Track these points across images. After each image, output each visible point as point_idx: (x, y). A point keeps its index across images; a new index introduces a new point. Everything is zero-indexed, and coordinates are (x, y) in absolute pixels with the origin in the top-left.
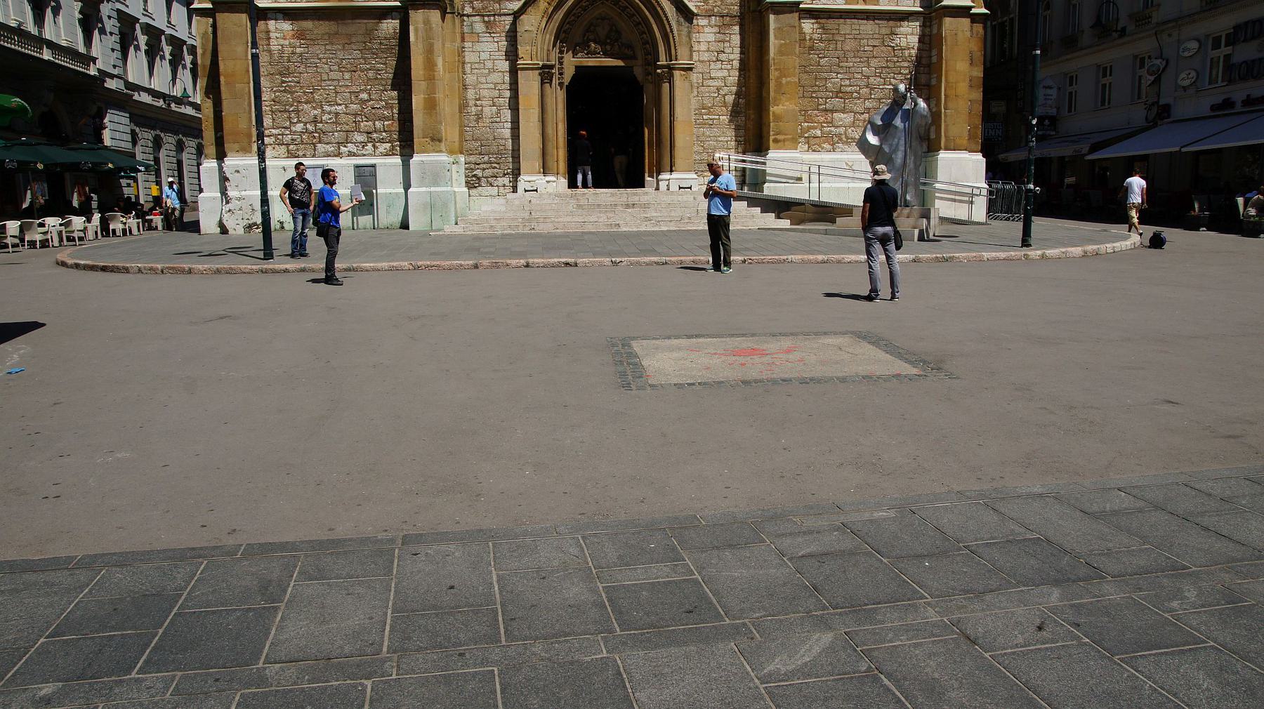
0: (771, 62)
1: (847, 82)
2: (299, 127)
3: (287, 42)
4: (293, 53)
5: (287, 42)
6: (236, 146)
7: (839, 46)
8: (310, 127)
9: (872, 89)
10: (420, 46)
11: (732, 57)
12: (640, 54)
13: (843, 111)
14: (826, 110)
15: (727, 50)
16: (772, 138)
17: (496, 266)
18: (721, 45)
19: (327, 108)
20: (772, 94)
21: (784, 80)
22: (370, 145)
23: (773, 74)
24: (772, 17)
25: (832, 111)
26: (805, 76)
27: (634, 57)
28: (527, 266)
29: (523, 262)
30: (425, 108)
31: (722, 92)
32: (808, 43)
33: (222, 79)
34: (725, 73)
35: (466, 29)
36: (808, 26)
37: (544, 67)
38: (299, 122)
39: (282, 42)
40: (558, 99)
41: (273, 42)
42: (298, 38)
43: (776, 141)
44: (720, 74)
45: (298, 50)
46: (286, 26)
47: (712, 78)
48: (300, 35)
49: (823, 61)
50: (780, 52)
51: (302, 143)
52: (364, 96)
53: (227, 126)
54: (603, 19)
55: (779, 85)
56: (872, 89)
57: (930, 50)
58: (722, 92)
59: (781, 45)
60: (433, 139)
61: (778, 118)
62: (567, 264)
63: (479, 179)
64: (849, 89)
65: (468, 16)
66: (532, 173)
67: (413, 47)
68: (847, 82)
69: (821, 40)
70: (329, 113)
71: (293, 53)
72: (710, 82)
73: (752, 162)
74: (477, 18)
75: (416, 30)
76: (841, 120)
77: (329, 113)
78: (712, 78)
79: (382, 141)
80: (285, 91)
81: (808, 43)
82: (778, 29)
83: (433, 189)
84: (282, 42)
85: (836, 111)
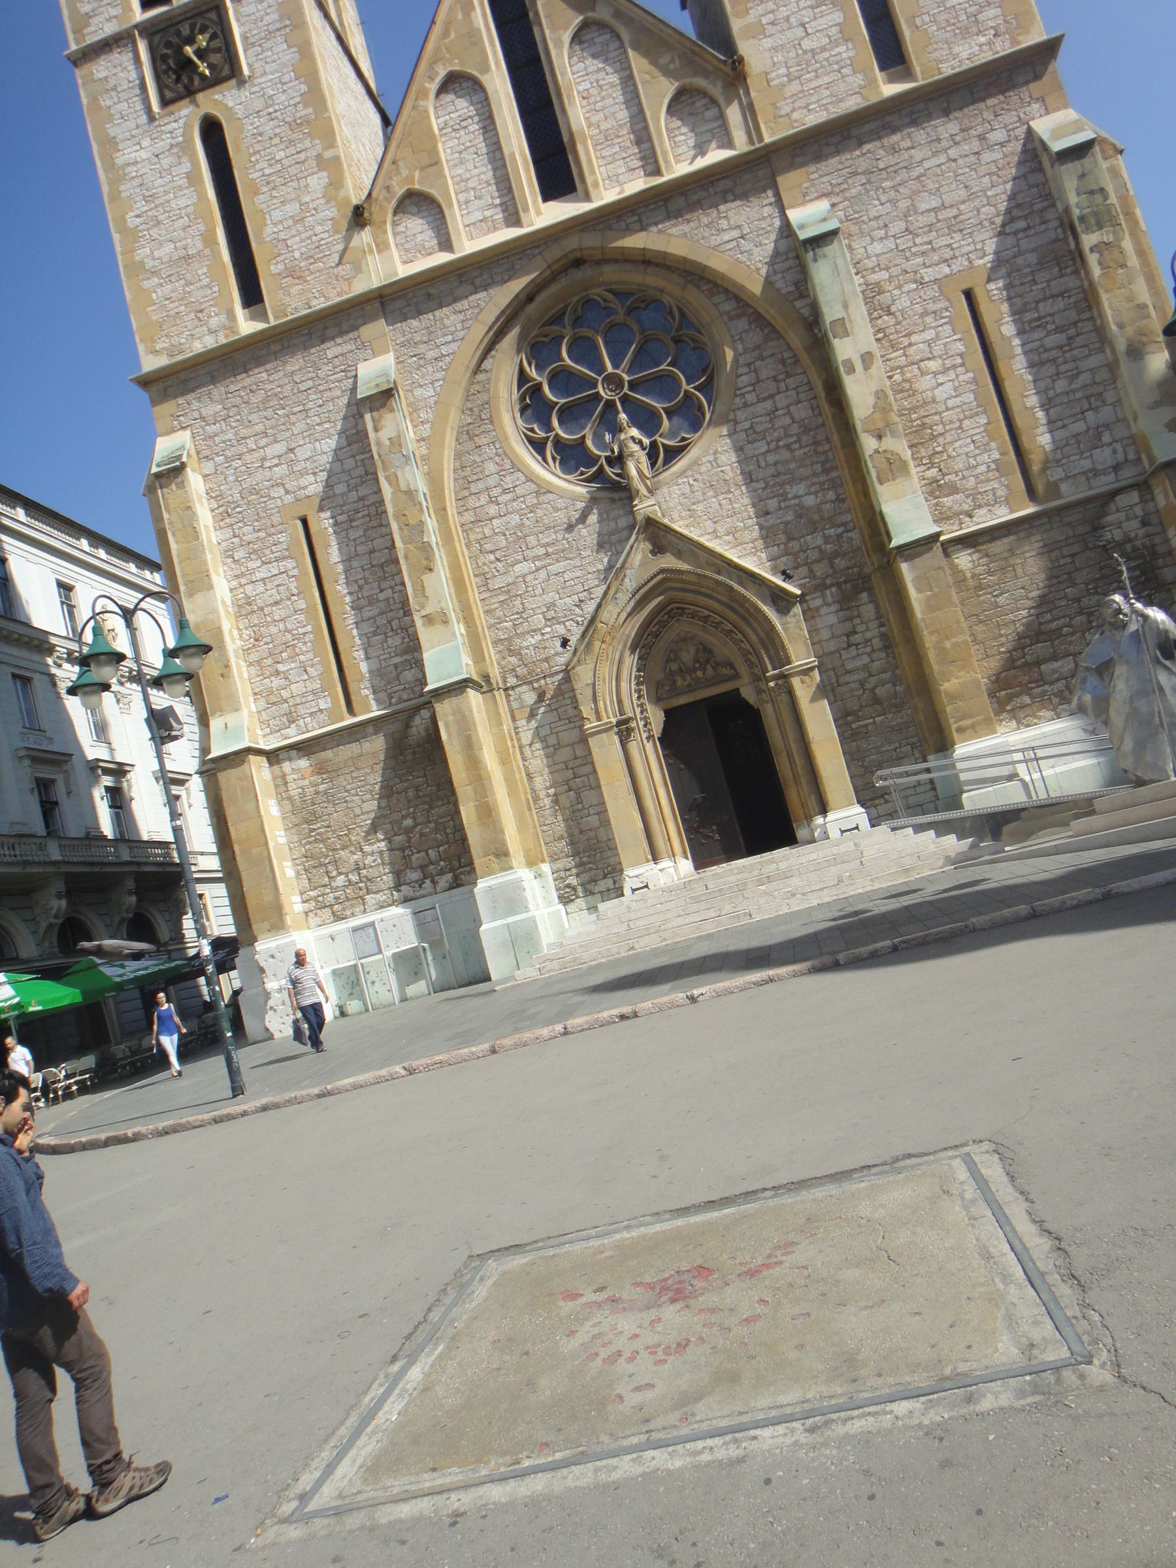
0: (922, 625)
1: (1048, 617)
2: (340, 881)
3: (307, 782)
4: (317, 793)
5: (307, 782)
6: (266, 925)
7: (1019, 571)
8: (354, 878)
9: (1090, 614)
10: (456, 742)
11: (868, 635)
12: (743, 669)
13: (1055, 658)
14: (1026, 664)
15: (859, 629)
16: (954, 727)
17: (411, 1072)
18: (848, 625)
19: (367, 848)
20: (936, 667)
21: (948, 644)
22: (428, 881)
23: (929, 641)
24: (904, 567)
25: (1039, 663)
26: (979, 629)
27: (737, 676)
28: (566, 1033)
29: (559, 1028)
30: (479, 819)
31: (868, 686)
32: (971, 583)
33: (236, 847)
34: (866, 659)
35: (515, 705)
36: (964, 560)
37: (619, 724)
38: (340, 874)
39: (301, 783)
40: (649, 759)
41: (292, 786)
42: (319, 773)
43: (961, 730)
44: (858, 663)
45: (322, 788)
46: (303, 763)
47: (848, 672)
48: (320, 769)
49: (1001, 600)
50: (930, 607)
51: (348, 899)
52: (408, 822)
53: (251, 903)
54: (684, 640)
55: (942, 651)
56: (1090, 614)
57: (1164, 531)
58: (868, 686)
59: (928, 599)
60: (497, 856)
61: (953, 697)
62: (623, 1017)
63: (574, 889)
64: (1054, 625)
65: (513, 688)
66: (637, 864)
67: (447, 747)
68: (1048, 617)
69: (990, 573)
70: (372, 854)
71: (317, 793)
72: (848, 678)
73: (900, 775)
74: (525, 688)
75: (447, 725)
76: (1054, 671)
77: (372, 854)
78: (848, 672)
79: (442, 873)
80: (316, 841)
81: (971, 583)
82: (917, 580)
83: (510, 920)
84: (301, 783)
85: (1045, 661)
